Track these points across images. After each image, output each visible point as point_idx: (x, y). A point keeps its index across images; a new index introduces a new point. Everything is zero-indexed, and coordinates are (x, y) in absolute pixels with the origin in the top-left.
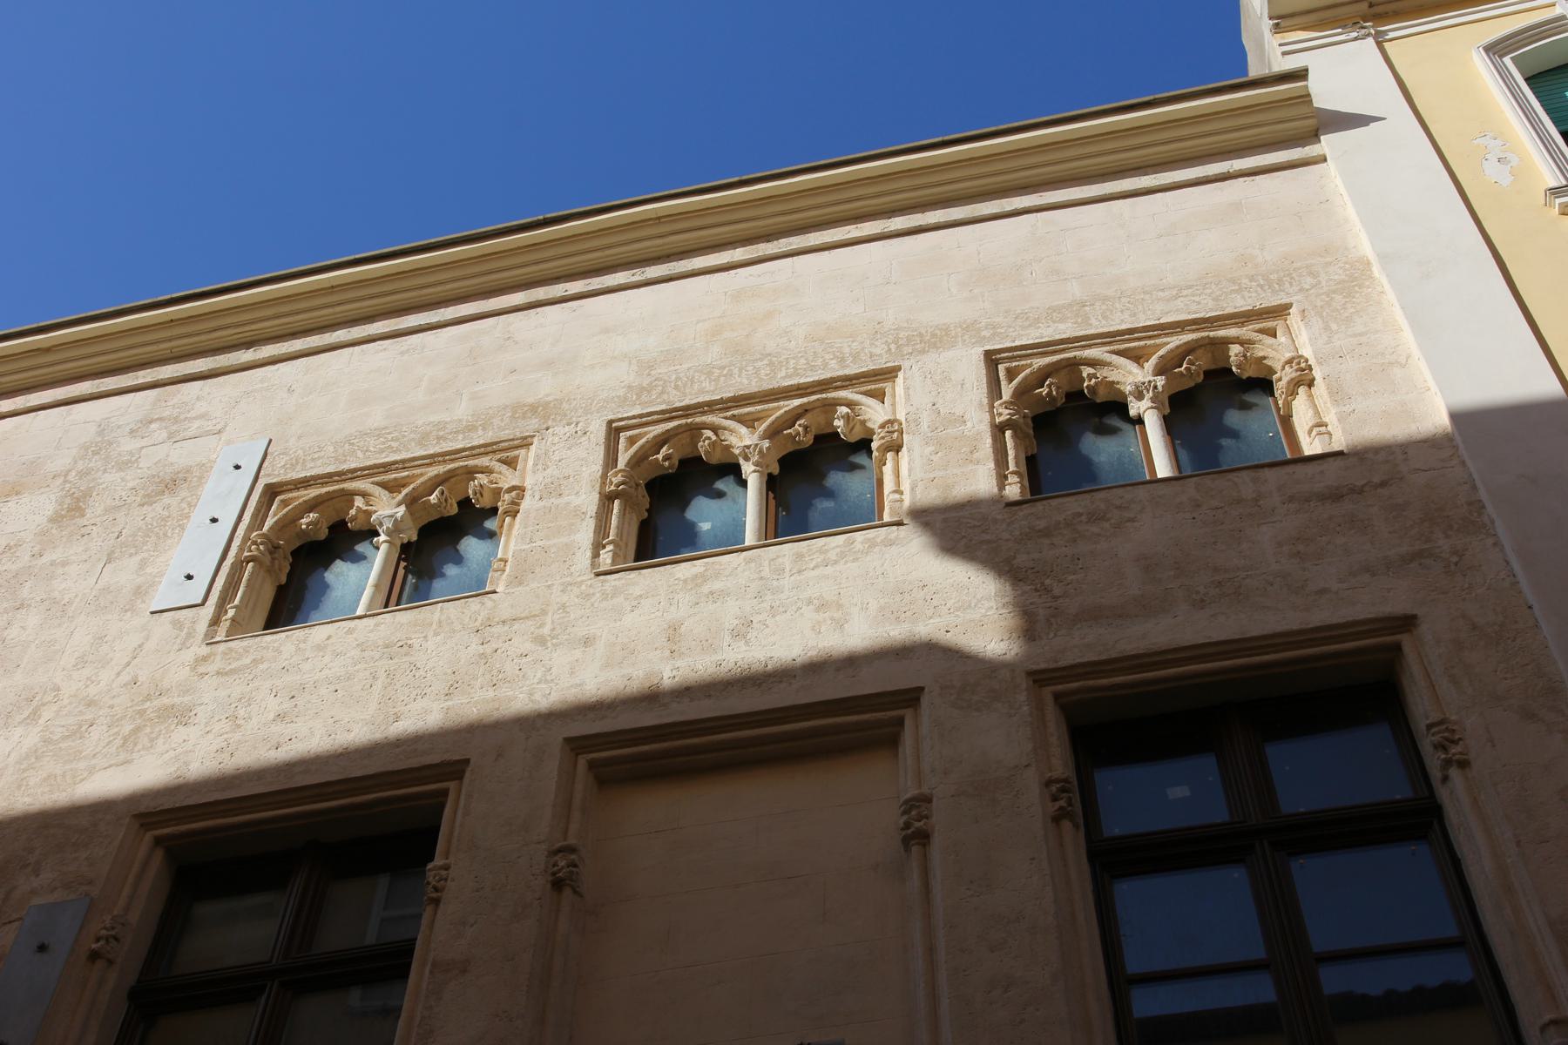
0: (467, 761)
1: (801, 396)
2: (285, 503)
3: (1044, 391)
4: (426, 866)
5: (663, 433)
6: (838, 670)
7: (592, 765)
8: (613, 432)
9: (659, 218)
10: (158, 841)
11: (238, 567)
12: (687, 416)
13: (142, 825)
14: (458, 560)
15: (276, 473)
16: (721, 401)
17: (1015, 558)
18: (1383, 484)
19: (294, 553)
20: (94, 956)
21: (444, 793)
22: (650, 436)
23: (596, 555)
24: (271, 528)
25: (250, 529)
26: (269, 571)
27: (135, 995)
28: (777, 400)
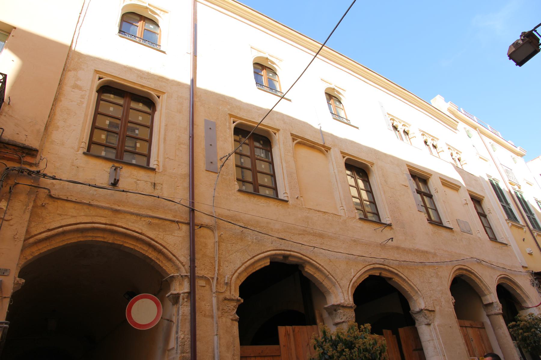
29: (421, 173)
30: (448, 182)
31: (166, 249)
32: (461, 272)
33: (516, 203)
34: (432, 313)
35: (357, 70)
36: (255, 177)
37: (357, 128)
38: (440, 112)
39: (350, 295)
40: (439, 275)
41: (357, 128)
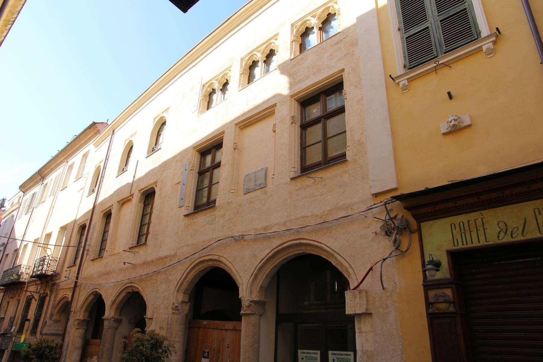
0: (224, 131)
1: (266, 43)
2: (296, 27)
3: (300, 29)
4: (342, 91)
5: (301, 24)
6: (266, 102)
7: (239, 127)
8: (292, 25)
9: (244, 11)
10: (196, 151)
11: (200, 102)
12: (251, 53)
13: (291, 97)
14: (332, 27)
15: (203, 83)
16: (255, 49)
17: (290, 72)
18: (345, 38)
19: (301, 36)
20: (191, 170)
21: (342, 75)
22: (247, 59)
23: (239, 87)
24: (295, 34)
25: (201, 94)
26: (205, 100)
27: (198, 173)
28: (263, 45)
29: (213, 141)
30: (252, 117)
31: (49, 299)
32: (206, 265)
33: (90, 225)
34: (151, 320)
35: (243, 16)
36: (316, 121)
37: (138, 161)
38: (118, 118)
39: (118, 303)
40: (169, 279)
41: (138, 161)
